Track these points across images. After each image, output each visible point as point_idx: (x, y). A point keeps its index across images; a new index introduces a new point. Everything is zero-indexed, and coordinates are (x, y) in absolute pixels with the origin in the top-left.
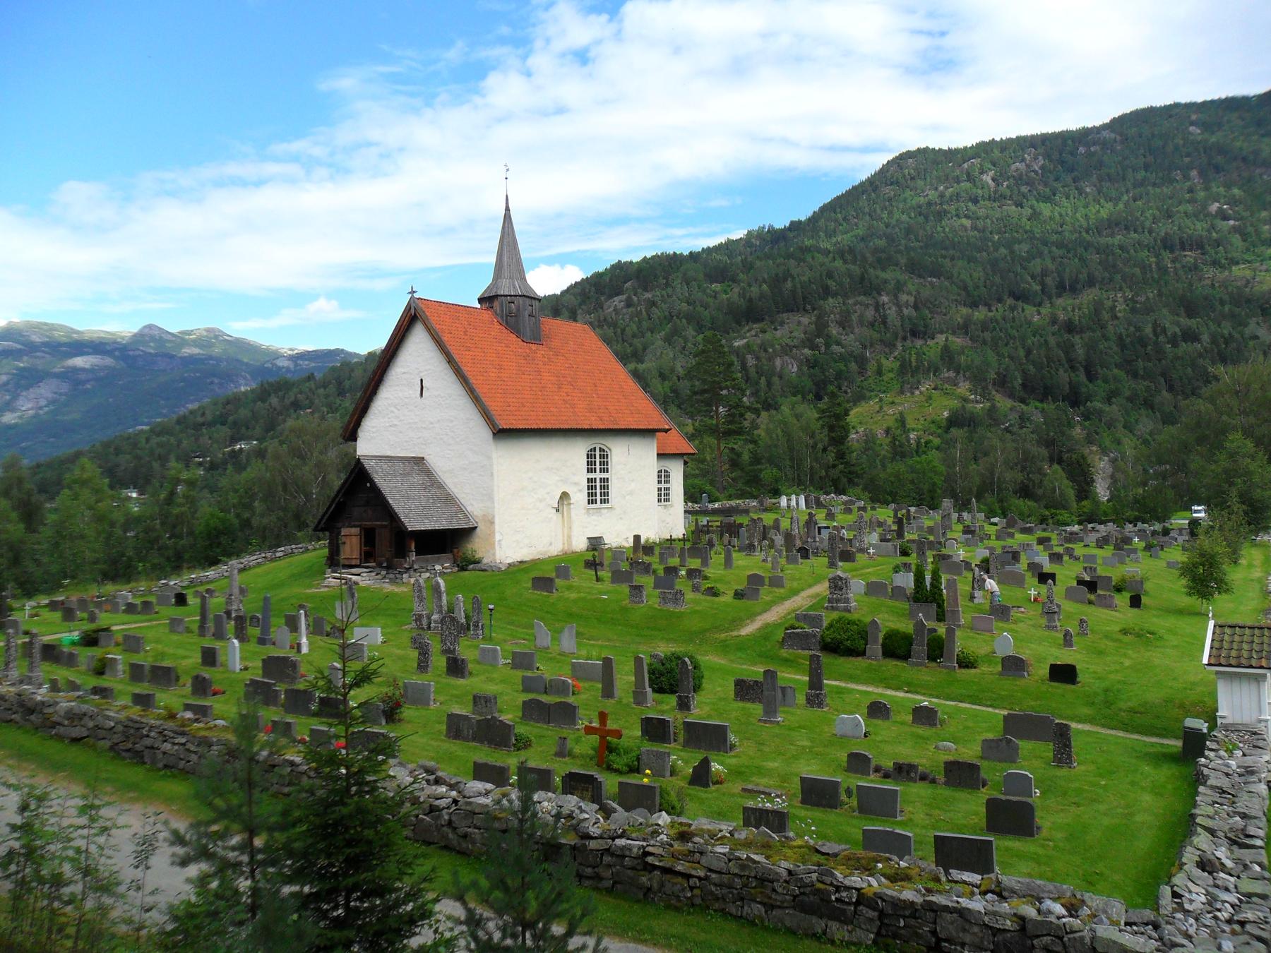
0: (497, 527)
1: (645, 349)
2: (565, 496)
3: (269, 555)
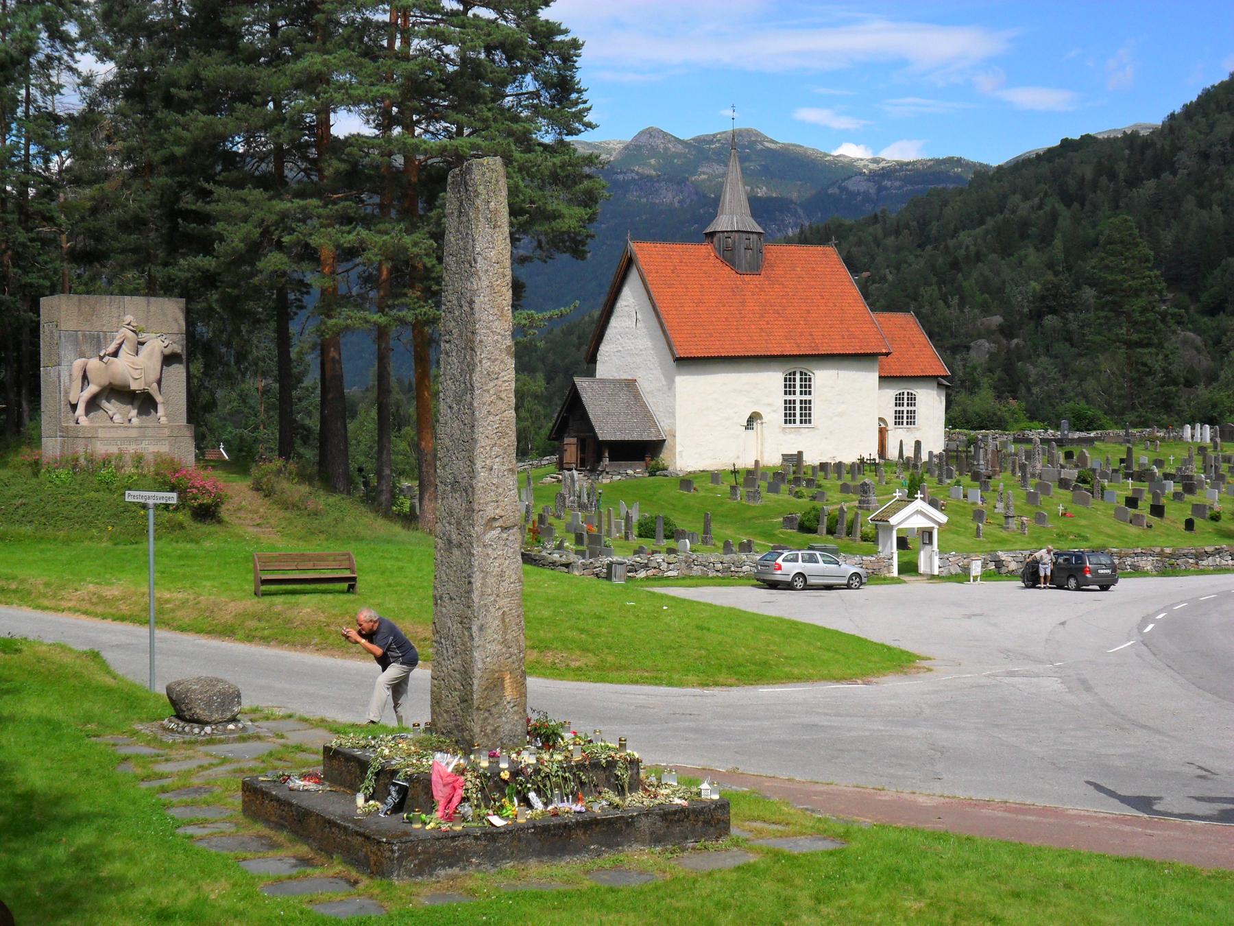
0: (678, 440)
3: (535, 462)
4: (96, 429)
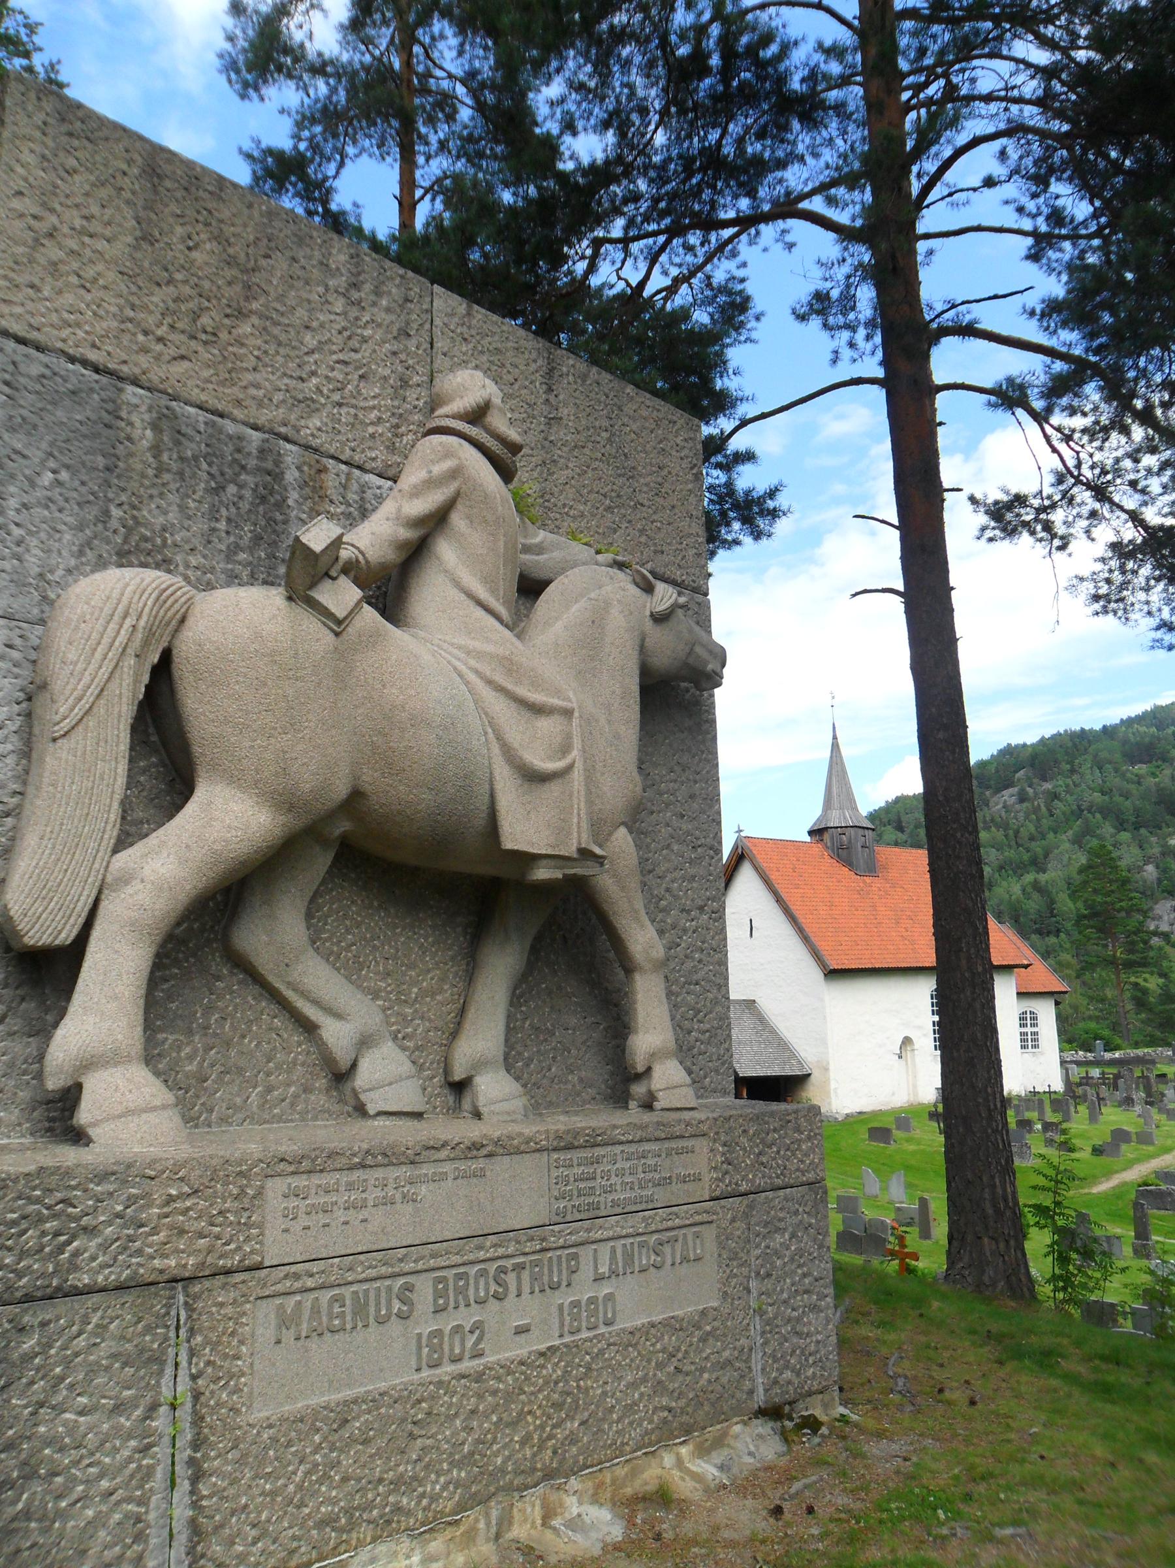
0: (832, 1074)
1: (1046, 856)
2: (907, 1041)
4: (241, 1183)
